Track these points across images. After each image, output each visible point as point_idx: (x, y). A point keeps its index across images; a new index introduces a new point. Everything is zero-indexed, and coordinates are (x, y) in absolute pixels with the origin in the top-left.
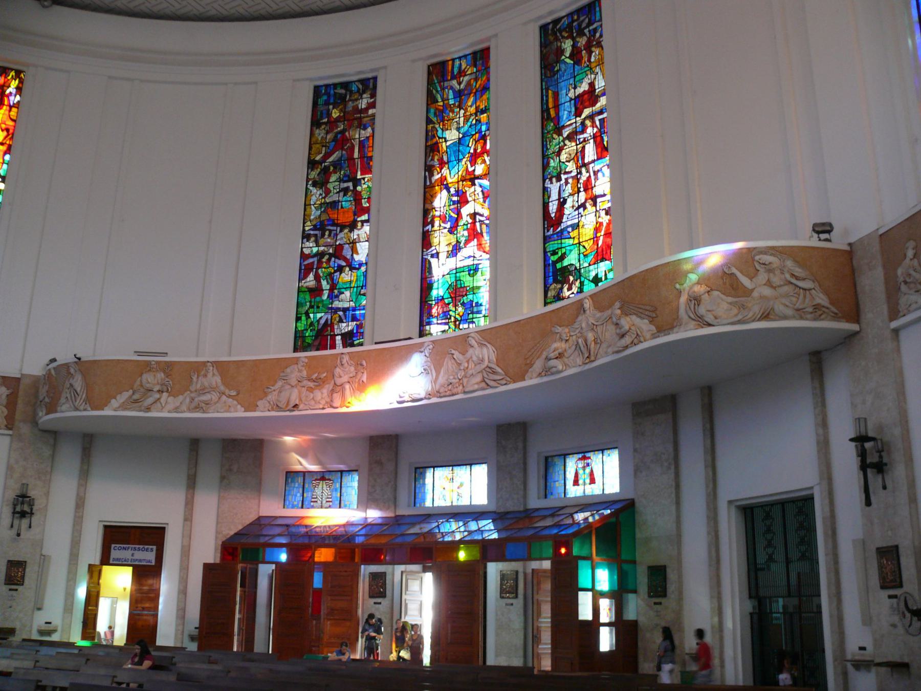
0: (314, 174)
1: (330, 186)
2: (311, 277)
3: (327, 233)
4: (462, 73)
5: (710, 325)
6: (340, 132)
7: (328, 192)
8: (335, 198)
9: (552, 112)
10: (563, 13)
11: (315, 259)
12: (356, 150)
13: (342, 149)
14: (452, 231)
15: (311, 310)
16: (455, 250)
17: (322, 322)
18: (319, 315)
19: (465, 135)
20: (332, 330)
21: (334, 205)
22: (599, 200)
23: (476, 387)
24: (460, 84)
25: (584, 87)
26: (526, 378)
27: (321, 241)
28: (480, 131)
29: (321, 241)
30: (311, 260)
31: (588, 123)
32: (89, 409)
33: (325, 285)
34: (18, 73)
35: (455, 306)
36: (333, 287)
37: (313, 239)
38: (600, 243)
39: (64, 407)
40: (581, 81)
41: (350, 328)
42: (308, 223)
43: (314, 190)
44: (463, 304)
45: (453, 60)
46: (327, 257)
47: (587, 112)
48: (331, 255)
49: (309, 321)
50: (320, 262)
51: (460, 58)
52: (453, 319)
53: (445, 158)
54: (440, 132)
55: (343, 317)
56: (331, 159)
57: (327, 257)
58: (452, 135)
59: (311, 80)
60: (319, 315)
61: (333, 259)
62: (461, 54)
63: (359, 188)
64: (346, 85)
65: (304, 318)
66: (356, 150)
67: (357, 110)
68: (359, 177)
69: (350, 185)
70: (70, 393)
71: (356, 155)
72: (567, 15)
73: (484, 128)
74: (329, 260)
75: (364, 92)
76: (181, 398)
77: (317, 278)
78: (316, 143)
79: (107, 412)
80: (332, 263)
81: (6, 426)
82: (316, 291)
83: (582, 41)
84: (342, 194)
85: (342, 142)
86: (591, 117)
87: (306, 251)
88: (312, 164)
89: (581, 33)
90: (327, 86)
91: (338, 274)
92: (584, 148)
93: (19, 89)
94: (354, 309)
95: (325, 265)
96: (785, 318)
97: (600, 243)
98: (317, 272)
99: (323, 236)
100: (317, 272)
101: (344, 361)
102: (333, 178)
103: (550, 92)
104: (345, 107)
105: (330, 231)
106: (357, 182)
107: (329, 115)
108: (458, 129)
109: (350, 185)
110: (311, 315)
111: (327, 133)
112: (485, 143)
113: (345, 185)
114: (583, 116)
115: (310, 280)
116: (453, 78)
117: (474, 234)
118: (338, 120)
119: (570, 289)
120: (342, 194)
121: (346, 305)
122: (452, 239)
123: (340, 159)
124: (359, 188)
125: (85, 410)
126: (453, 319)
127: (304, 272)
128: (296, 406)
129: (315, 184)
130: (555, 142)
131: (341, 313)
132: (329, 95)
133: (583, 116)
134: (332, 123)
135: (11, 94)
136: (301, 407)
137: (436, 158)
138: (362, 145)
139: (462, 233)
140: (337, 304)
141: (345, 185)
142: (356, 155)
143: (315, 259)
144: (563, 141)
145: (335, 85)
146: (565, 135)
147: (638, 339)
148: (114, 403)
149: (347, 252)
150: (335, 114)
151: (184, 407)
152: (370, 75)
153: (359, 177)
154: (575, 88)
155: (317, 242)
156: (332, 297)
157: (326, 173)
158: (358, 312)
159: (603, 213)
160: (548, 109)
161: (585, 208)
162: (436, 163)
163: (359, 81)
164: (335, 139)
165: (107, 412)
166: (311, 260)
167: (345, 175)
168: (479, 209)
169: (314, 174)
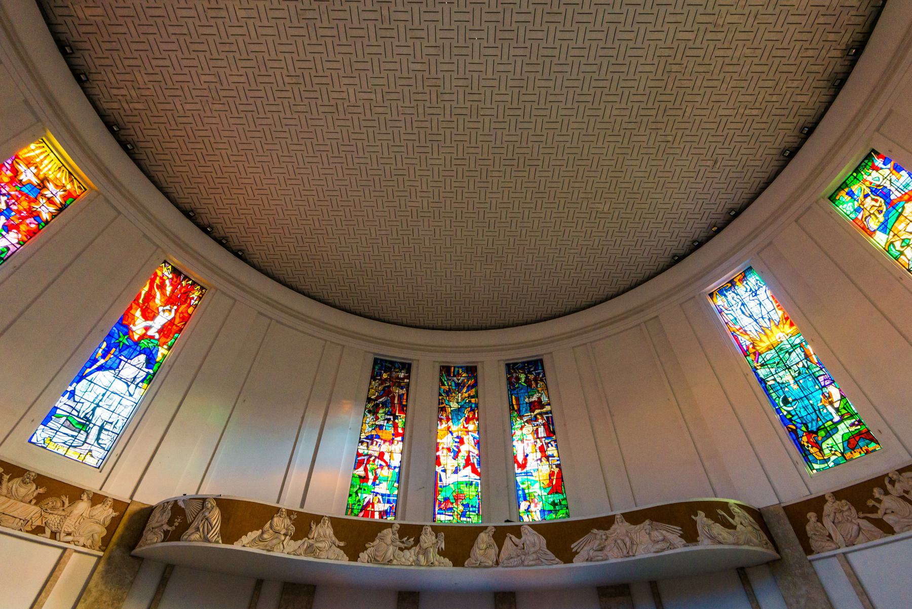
0: (370, 406)
1: (379, 415)
2: (362, 468)
3: (375, 443)
4: (459, 375)
5: (720, 543)
6: (388, 387)
7: (377, 418)
8: (382, 423)
9: (516, 407)
10: (520, 361)
11: (366, 458)
12: (396, 399)
13: (388, 396)
14: (455, 457)
15: (360, 491)
16: (456, 471)
17: (367, 500)
18: (364, 496)
19: (462, 407)
20: (373, 507)
21: (381, 427)
22: (550, 459)
23: (533, 563)
24: (458, 380)
25: (535, 398)
26: (574, 560)
27: (371, 447)
28: (471, 407)
29: (371, 447)
30: (363, 458)
31: (539, 417)
32: (220, 542)
33: (371, 476)
34: (202, 288)
35: (457, 504)
36: (376, 478)
37: (365, 444)
38: (554, 483)
39: (193, 537)
40: (532, 395)
41: (386, 508)
42: (363, 434)
43: (369, 415)
44: (463, 505)
45: (454, 367)
46: (373, 458)
47: (537, 411)
48: (376, 457)
49: (358, 498)
50: (368, 461)
51: (458, 367)
52: (456, 513)
53: (450, 417)
54: (447, 402)
55: (381, 500)
56: (381, 400)
57: (373, 458)
58: (454, 405)
59: (375, 354)
60: (364, 496)
61: (377, 460)
62: (459, 365)
63: (396, 421)
64: (392, 363)
65: (354, 495)
66: (396, 399)
67: (398, 378)
68: (397, 414)
69: (392, 417)
70: (204, 525)
71: (396, 402)
72: (522, 363)
73: (473, 406)
74: (374, 461)
75: (402, 369)
76: (300, 542)
77: (366, 470)
78: (372, 388)
79: (237, 546)
80: (376, 462)
81: (100, 548)
82: (364, 479)
83: (531, 377)
84: (386, 421)
85: (387, 392)
86: (541, 414)
87: (361, 451)
88: (369, 400)
89: (531, 373)
90: (381, 360)
91: (379, 470)
92: (537, 429)
93: (200, 298)
94: (389, 496)
95: (371, 462)
96: (755, 545)
97: (554, 483)
98: (366, 466)
99: (372, 444)
100: (366, 466)
101: (428, 532)
102: (381, 411)
103: (513, 397)
104: (391, 374)
105: (377, 442)
106: (395, 417)
107: (381, 376)
108: (458, 403)
109: (392, 417)
110: (359, 494)
111: (379, 385)
112: (474, 414)
113: (389, 417)
114: (535, 413)
115: (361, 471)
116: (454, 376)
117: (468, 462)
118: (386, 379)
119: (536, 506)
120: (386, 421)
121: (384, 492)
122: (455, 463)
123: (386, 401)
124: (396, 421)
125: (217, 542)
126: (456, 513)
127: (358, 464)
128: (390, 561)
129: (369, 412)
130: (518, 422)
131: (380, 497)
132: (382, 365)
133: (535, 413)
134: (383, 381)
135: (193, 298)
136: (395, 562)
137: (444, 415)
138: (400, 397)
139: (461, 461)
140: (377, 489)
141: (389, 417)
142: (396, 402)
143: (366, 458)
144: (524, 423)
145: (386, 361)
146: (525, 420)
147: (672, 546)
148: (245, 540)
149: (386, 457)
150: (385, 376)
151: (302, 551)
152: (407, 362)
153: (397, 414)
154: (529, 398)
155: (368, 447)
156: (374, 484)
157: (377, 406)
158: (391, 498)
159: (554, 466)
160: (513, 405)
161: (541, 461)
162: (444, 417)
163: (400, 363)
164: (384, 389)
165: (237, 546)
166: (363, 458)
167: (388, 411)
168: (472, 449)
169: (370, 406)
